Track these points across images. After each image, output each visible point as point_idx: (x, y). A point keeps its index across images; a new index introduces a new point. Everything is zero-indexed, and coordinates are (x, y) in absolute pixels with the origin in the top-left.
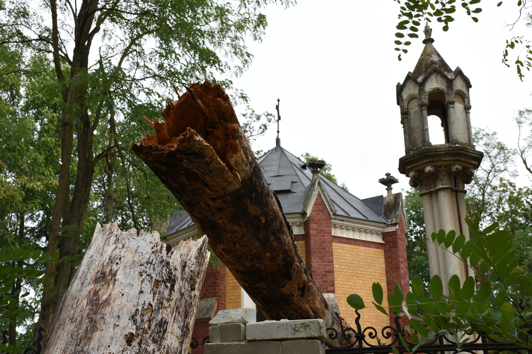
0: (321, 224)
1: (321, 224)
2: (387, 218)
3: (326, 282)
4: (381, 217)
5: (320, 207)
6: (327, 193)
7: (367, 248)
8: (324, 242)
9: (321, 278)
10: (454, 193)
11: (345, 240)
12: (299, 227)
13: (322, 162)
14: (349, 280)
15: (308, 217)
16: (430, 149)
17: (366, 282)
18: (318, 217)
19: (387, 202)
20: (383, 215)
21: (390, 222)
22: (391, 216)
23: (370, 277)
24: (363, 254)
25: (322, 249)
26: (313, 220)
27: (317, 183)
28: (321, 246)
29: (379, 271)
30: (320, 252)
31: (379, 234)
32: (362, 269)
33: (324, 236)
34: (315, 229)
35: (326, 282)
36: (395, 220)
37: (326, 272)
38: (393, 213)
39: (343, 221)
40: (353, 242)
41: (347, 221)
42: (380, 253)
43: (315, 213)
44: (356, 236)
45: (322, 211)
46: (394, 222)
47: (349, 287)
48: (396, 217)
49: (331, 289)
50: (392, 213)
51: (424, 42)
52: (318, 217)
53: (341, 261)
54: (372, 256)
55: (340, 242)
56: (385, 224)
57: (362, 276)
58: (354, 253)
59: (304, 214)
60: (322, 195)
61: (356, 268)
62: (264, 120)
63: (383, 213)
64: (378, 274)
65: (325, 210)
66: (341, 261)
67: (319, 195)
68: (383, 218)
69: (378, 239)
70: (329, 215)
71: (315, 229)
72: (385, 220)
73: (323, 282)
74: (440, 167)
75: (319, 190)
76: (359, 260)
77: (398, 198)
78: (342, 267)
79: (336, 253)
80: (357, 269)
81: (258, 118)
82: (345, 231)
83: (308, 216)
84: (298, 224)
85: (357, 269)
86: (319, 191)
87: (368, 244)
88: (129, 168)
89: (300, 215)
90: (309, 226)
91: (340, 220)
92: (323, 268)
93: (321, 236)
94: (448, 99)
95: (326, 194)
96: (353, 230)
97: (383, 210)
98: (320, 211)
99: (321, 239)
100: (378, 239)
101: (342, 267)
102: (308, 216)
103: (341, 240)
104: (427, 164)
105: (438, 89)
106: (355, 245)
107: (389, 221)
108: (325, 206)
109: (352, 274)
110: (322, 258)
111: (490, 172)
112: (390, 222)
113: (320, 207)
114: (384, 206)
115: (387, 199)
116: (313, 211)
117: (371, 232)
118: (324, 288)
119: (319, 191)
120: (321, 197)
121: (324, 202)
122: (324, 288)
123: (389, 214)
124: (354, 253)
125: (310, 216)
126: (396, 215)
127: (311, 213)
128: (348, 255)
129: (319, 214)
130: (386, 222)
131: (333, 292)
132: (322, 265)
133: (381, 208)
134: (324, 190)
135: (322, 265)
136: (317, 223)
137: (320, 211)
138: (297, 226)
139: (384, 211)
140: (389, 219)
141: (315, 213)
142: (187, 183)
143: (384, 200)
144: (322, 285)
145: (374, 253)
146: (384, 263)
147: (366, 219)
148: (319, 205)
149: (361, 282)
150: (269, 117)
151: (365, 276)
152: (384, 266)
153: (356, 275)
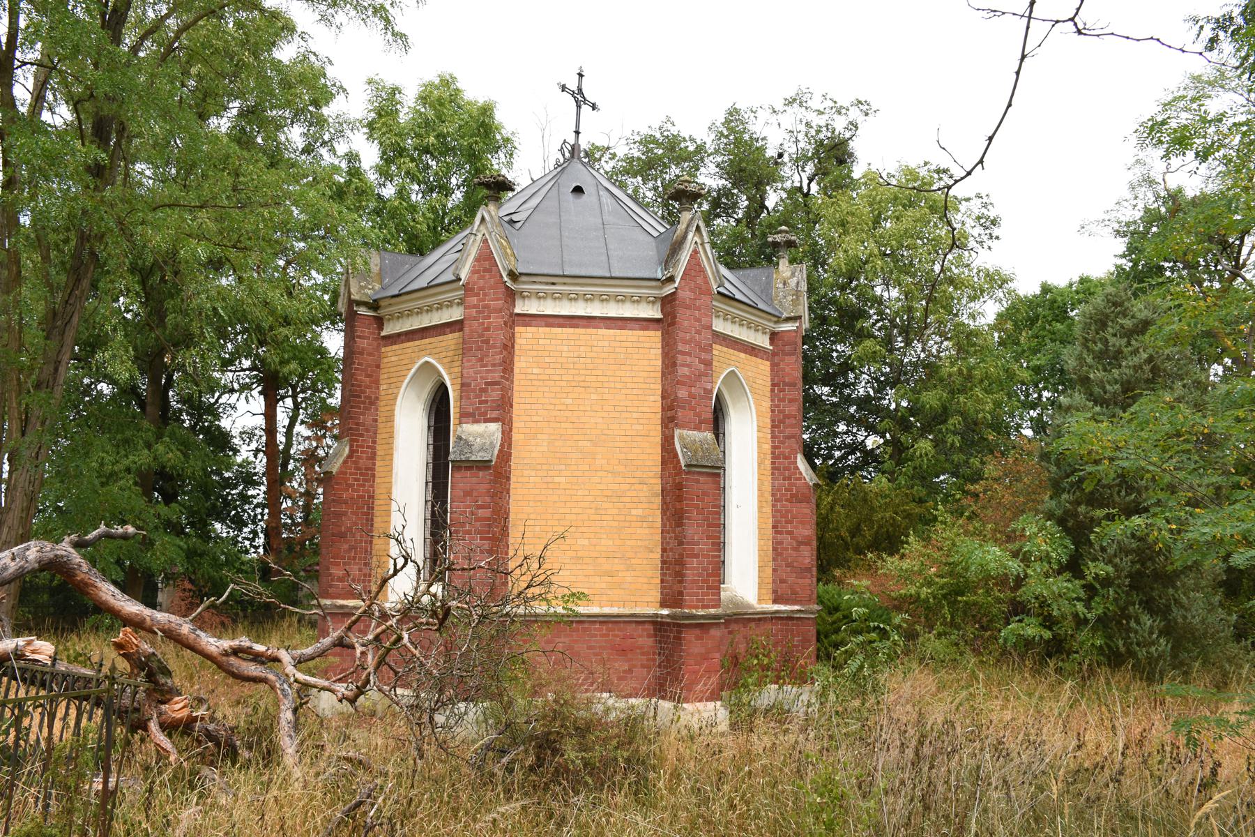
0: (485, 295)
1: (485, 295)
3: (486, 402)
7: (618, 332)
8: (488, 329)
9: (476, 396)
11: (561, 321)
14: (564, 395)
17: (605, 397)
23: (618, 385)
24: (606, 344)
25: (483, 342)
28: (483, 335)
29: (453, 347)
30: (480, 349)
31: (653, 303)
32: (600, 373)
33: (489, 317)
34: (474, 307)
35: (486, 402)
37: (487, 384)
39: (553, 284)
40: (584, 322)
42: (653, 338)
44: (595, 310)
47: (564, 407)
53: (547, 360)
54: (630, 345)
55: (548, 325)
57: (599, 385)
58: (582, 343)
61: (582, 372)
64: (642, 380)
66: (547, 360)
69: (654, 312)
73: (481, 402)
76: (594, 355)
78: (547, 371)
79: (765, 378)
80: (588, 372)
82: (752, 332)
85: (588, 372)
87: (620, 323)
91: (547, 283)
92: (481, 378)
93: (484, 318)
98: (485, 271)
99: (483, 324)
100: (763, 341)
101: (547, 371)
103: (551, 320)
106: (584, 327)
109: (574, 384)
110: (481, 360)
116: (473, 272)
117: (638, 300)
118: (480, 415)
122: (480, 415)
124: (582, 343)
128: (566, 348)
129: (483, 277)
132: (480, 372)
135: (480, 372)
136: (478, 295)
137: (485, 271)
144: (478, 409)
145: (634, 339)
146: (660, 357)
149: (594, 396)
151: (606, 385)
152: (659, 363)
153: (582, 384)
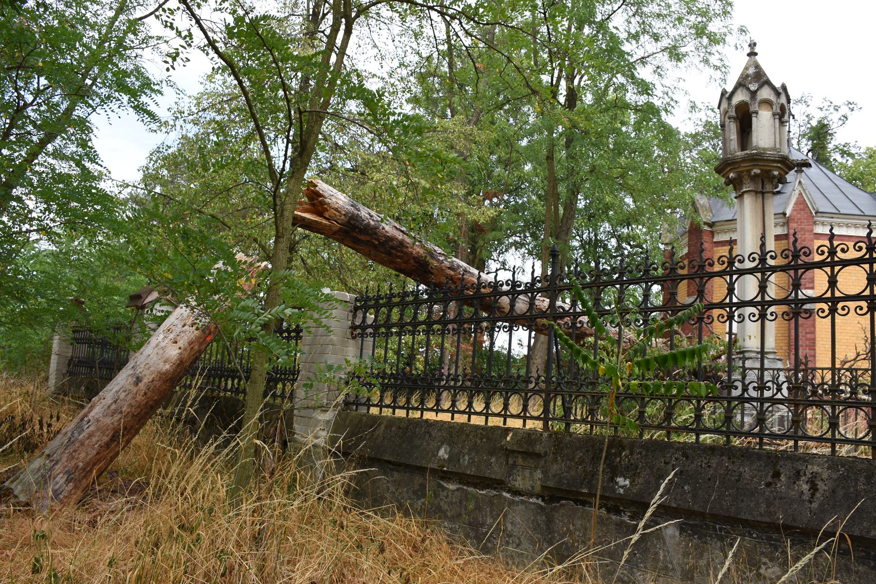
5: (802, 206)
10: (760, 196)
16: (756, 154)
18: (799, 216)
45: (803, 210)
49: (811, 285)
51: (749, 55)
52: (799, 216)
59: (784, 214)
62: (844, 110)
67: (800, 194)
74: (742, 172)
81: (836, 109)
88: (95, 209)
94: (752, 109)
96: (847, 226)
104: (730, 171)
105: (743, 101)
113: (802, 206)
116: (794, 210)
117: (856, 226)
125: (790, 216)
131: (813, 288)
148: (801, 204)
150: (851, 106)
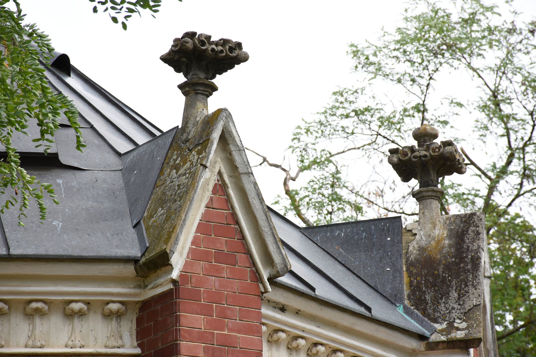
0: (223, 314)
1: (223, 314)
2: (425, 313)
4: (400, 310)
6: (255, 184)
12: (114, 323)
13: (231, 49)
15: (174, 282)
18: (213, 282)
19: (422, 249)
20: (406, 302)
21: (441, 332)
22: (442, 307)
26: (195, 296)
27: (216, 135)
34: (201, 337)
36: (464, 325)
38: (454, 295)
39: (283, 309)
41: (297, 313)
43: (200, 267)
46: (460, 335)
48: (467, 315)
50: (447, 294)
52: (213, 282)
56: (422, 338)
60: (231, 192)
63: (406, 291)
65: (241, 257)
68: (407, 310)
70: (257, 277)
71: (201, 337)
72: (421, 323)
75: (220, 165)
77: (471, 234)
83: (175, 275)
84: (114, 307)
86: (220, 173)
89: (129, 270)
90: (177, 318)
95: (249, 187)
97: (406, 279)
98: (220, 257)
102: (175, 275)
107: (438, 326)
108: (243, 237)
111: (503, 172)
112: (441, 332)
114: (410, 265)
115: (421, 239)
119: (220, 173)
120: (228, 200)
121: (237, 223)
123: (436, 301)
126: (467, 307)
127: (186, 264)
129: (215, 272)
130: (427, 333)
133: (397, 271)
134: (241, 169)
136: (207, 311)
137: (220, 257)
138: (108, 316)
139: (411, 284)
140: (435, 321)
141: (200, 267)
142: (206, 47)
143: (406, 237)
147: (362, 310)
